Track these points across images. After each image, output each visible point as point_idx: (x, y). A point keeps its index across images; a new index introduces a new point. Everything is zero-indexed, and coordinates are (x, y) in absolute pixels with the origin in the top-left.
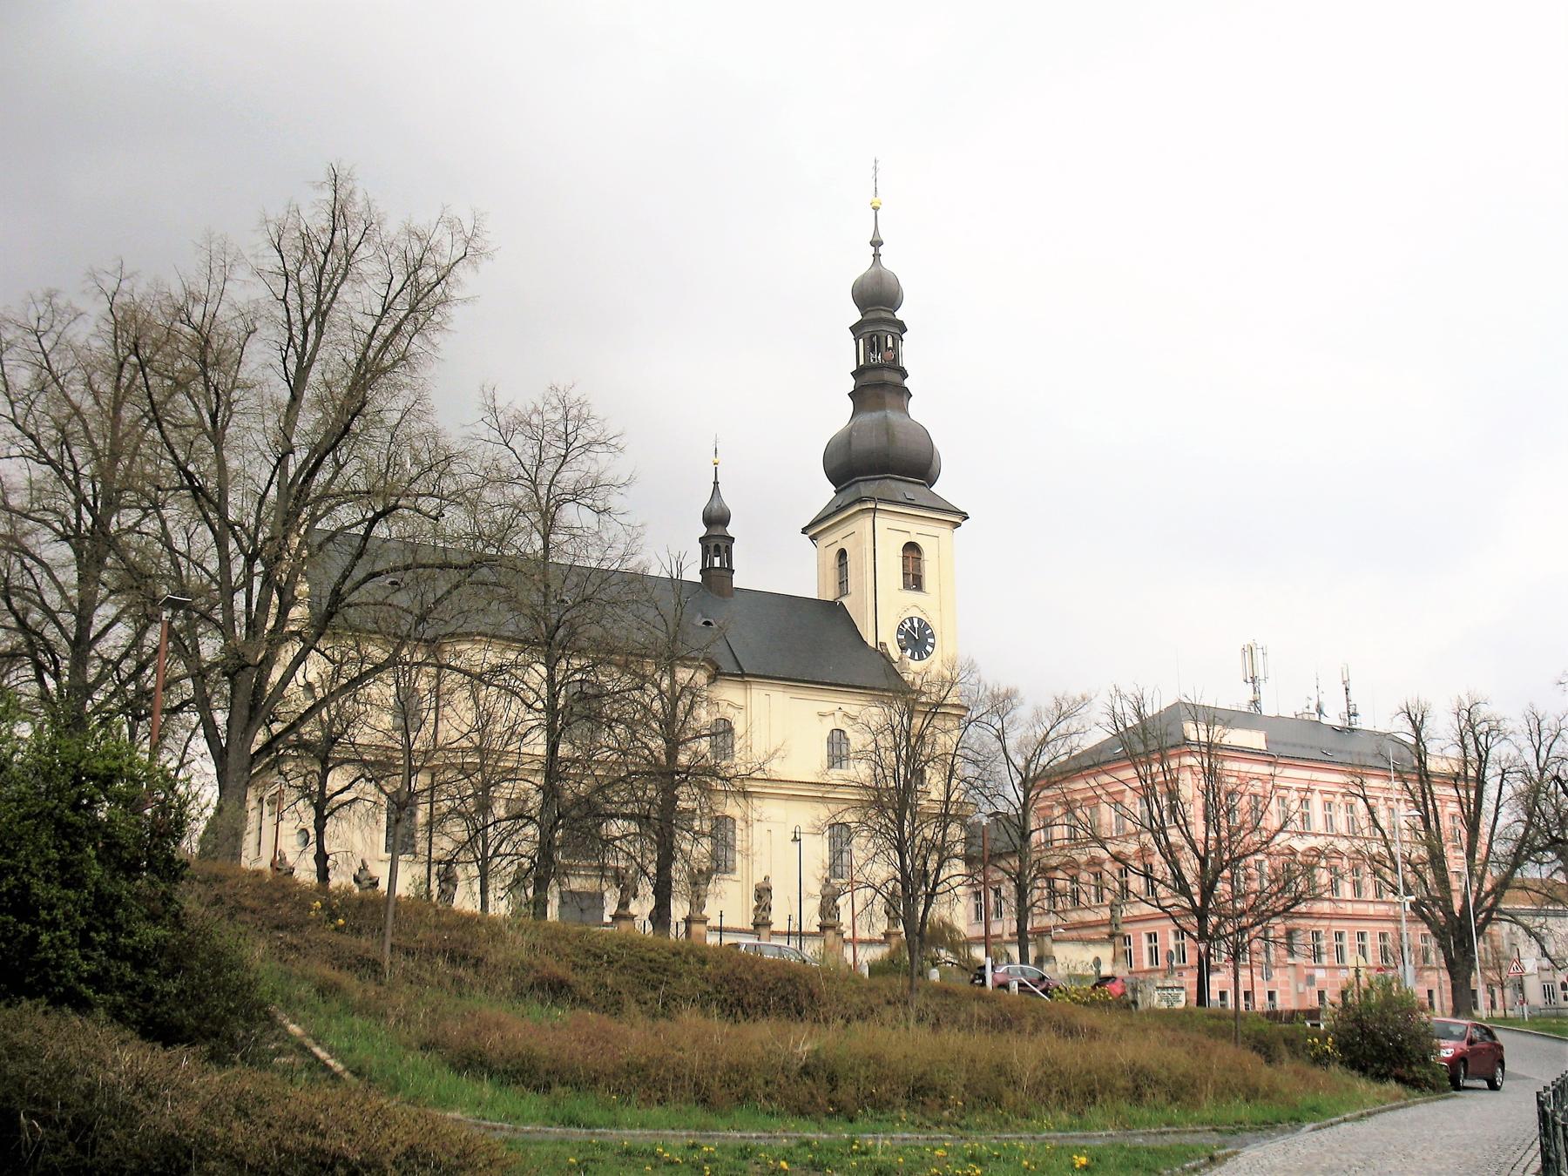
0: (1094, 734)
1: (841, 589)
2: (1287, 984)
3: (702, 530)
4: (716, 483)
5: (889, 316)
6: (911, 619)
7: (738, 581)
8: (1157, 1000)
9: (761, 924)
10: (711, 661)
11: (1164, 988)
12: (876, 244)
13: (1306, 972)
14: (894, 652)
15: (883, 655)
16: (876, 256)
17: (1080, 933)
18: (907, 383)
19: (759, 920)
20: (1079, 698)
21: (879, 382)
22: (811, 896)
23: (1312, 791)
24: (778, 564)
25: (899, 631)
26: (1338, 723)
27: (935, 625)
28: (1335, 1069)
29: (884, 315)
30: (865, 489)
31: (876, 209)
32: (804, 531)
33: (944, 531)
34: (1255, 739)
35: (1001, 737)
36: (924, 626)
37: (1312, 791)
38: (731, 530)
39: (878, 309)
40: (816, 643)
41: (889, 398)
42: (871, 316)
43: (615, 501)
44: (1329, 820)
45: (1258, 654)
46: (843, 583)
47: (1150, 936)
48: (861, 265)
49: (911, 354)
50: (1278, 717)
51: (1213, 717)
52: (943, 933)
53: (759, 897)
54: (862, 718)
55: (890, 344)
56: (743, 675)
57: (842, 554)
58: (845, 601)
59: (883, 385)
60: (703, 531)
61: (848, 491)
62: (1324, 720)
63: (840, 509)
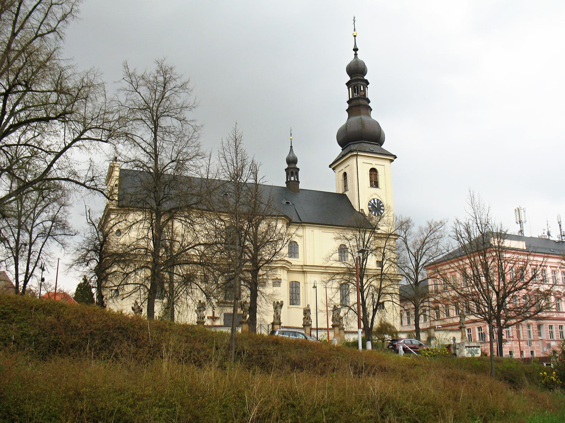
0: (449, 244)
1: (345, 189)
2: (539, 347)
3: (286, 166)
4: (291, 147)
5: (362, 78)
6: (374, 199)
7: (301, 186)
8: (466, 353)
9: (307, 324)
10: (286, 216)
11: (469, 347)
12: (356, 50)
13: (547, 342)
14: (367, 212)
15: (362, 214)
16: (356, 55)
17: (446, 328)
18: (370, 105)
19: (305, 323)
20: (438, 222)
21: (358, 104)
22: (321, 311)
23: (546, 266)
24: (318, 177)
25: (369, 204)
26: (557, 239)
27: (384, 202)
28: (558, 391)
29: (359, 77)
30: (353, 147)
31: (355, 36)
32: (330, 166)
33: (387, 163)
34: (521, 245)
35: (405, 241)
36: (380, 202)
37: (546, 266)
38: (298, 166)
39: (357, 74)
40: (335, 210)
41: (363, 110)
42: (353, 78)
43: (187, 114)
44: (554, 278)
45: (522, 212)
46: (346, 186)
47: (479, 328)
48: (350, 58)
49: (371, 93)
50: (531, 237)
51: (502, 236)
52: (386, 328)
53: (305, 313)
54: (351, 240)
55: (362, 89)
56: (302, 223)
57: (345, 174)
58: (347, 193)
59: (359, 105)
60: (286, 166)
61: (347, 149)
62: (551, 238)
63: (343, 156)
